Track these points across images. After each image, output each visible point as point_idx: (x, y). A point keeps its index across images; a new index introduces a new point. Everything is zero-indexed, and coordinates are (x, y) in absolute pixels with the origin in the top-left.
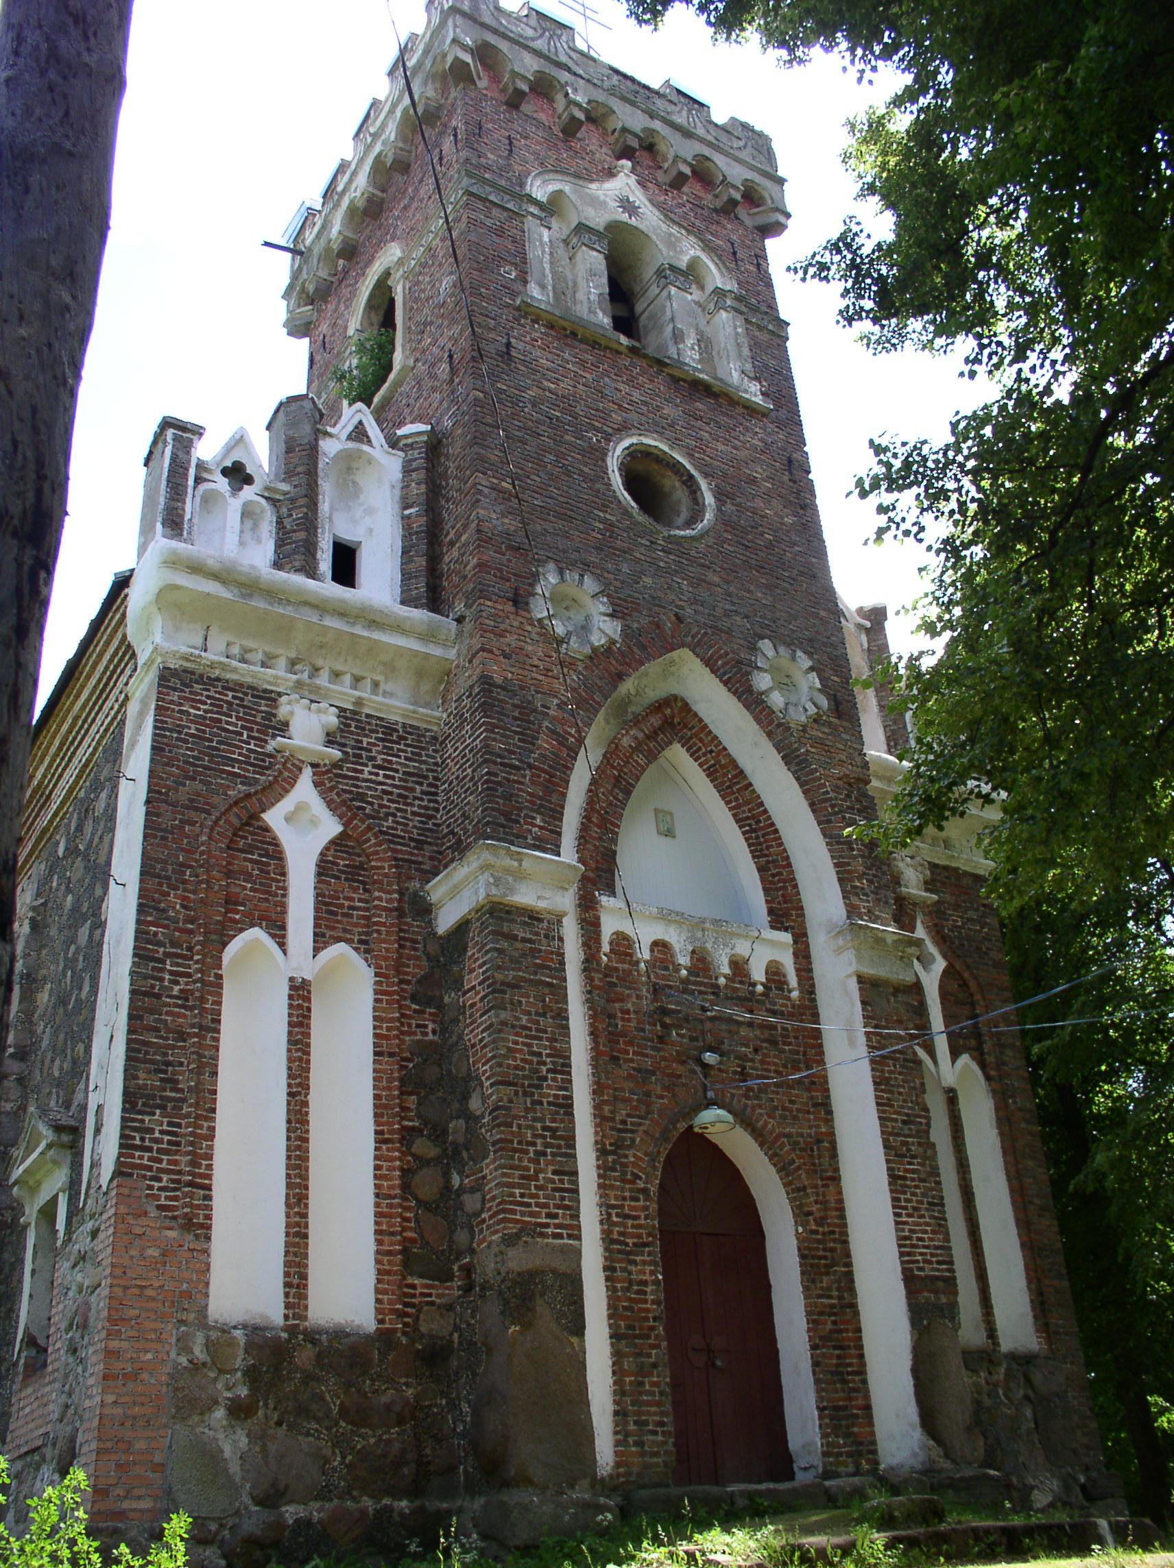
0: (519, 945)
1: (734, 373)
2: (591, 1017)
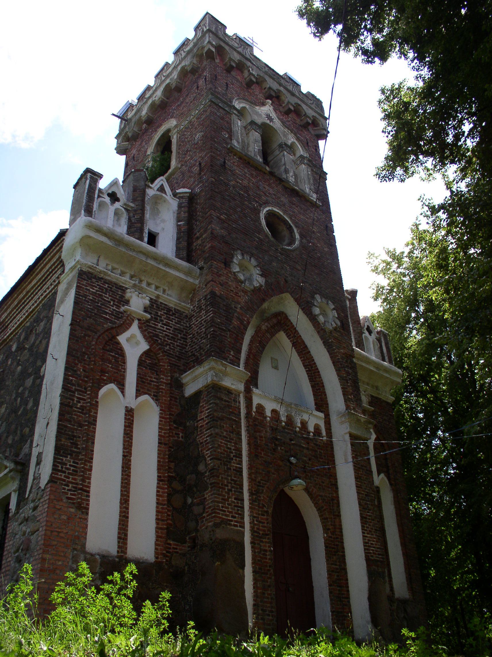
0: (223, 403)
1: (307, 188)
2: (248, 437)
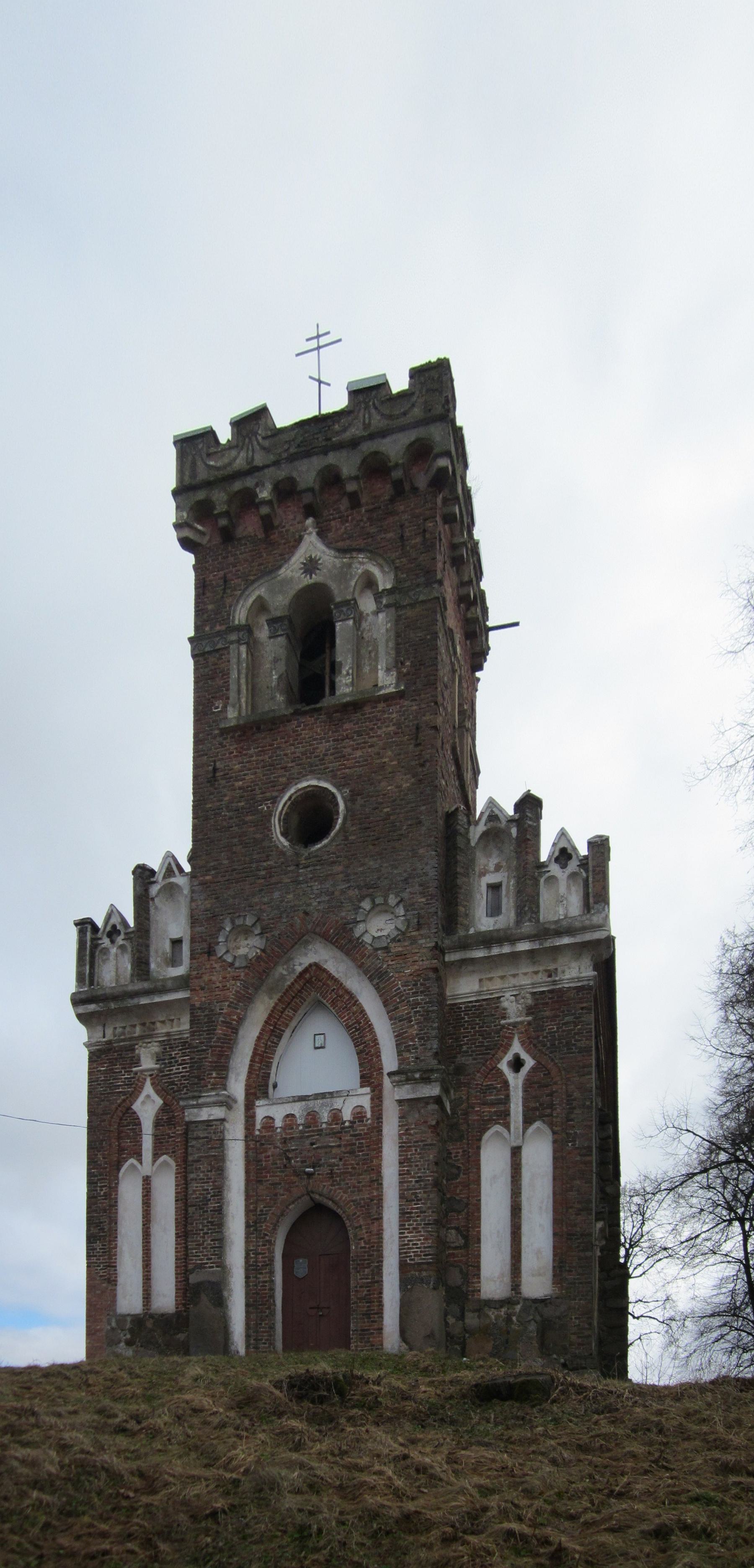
0: (200, 1141)
